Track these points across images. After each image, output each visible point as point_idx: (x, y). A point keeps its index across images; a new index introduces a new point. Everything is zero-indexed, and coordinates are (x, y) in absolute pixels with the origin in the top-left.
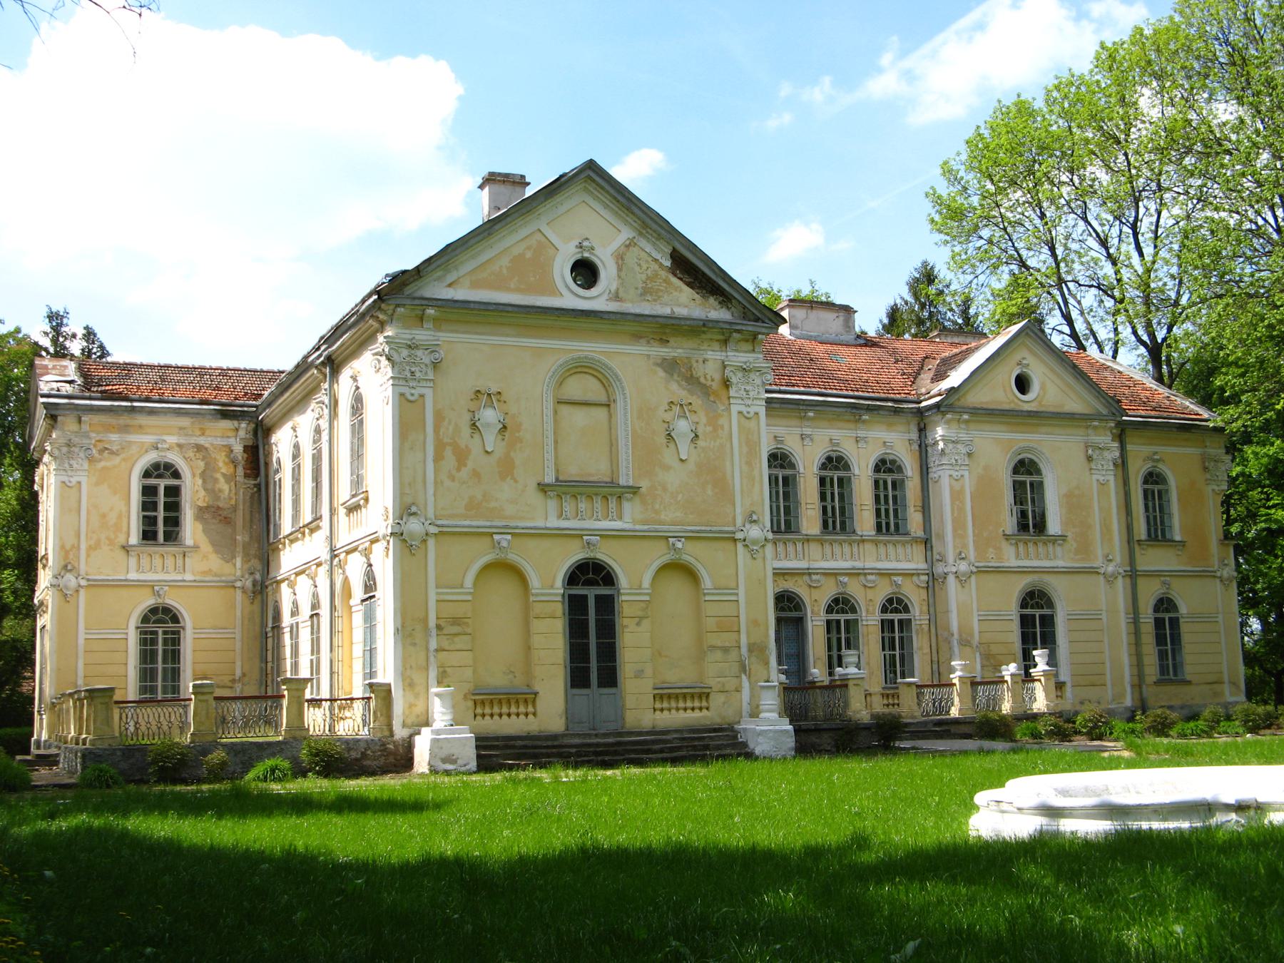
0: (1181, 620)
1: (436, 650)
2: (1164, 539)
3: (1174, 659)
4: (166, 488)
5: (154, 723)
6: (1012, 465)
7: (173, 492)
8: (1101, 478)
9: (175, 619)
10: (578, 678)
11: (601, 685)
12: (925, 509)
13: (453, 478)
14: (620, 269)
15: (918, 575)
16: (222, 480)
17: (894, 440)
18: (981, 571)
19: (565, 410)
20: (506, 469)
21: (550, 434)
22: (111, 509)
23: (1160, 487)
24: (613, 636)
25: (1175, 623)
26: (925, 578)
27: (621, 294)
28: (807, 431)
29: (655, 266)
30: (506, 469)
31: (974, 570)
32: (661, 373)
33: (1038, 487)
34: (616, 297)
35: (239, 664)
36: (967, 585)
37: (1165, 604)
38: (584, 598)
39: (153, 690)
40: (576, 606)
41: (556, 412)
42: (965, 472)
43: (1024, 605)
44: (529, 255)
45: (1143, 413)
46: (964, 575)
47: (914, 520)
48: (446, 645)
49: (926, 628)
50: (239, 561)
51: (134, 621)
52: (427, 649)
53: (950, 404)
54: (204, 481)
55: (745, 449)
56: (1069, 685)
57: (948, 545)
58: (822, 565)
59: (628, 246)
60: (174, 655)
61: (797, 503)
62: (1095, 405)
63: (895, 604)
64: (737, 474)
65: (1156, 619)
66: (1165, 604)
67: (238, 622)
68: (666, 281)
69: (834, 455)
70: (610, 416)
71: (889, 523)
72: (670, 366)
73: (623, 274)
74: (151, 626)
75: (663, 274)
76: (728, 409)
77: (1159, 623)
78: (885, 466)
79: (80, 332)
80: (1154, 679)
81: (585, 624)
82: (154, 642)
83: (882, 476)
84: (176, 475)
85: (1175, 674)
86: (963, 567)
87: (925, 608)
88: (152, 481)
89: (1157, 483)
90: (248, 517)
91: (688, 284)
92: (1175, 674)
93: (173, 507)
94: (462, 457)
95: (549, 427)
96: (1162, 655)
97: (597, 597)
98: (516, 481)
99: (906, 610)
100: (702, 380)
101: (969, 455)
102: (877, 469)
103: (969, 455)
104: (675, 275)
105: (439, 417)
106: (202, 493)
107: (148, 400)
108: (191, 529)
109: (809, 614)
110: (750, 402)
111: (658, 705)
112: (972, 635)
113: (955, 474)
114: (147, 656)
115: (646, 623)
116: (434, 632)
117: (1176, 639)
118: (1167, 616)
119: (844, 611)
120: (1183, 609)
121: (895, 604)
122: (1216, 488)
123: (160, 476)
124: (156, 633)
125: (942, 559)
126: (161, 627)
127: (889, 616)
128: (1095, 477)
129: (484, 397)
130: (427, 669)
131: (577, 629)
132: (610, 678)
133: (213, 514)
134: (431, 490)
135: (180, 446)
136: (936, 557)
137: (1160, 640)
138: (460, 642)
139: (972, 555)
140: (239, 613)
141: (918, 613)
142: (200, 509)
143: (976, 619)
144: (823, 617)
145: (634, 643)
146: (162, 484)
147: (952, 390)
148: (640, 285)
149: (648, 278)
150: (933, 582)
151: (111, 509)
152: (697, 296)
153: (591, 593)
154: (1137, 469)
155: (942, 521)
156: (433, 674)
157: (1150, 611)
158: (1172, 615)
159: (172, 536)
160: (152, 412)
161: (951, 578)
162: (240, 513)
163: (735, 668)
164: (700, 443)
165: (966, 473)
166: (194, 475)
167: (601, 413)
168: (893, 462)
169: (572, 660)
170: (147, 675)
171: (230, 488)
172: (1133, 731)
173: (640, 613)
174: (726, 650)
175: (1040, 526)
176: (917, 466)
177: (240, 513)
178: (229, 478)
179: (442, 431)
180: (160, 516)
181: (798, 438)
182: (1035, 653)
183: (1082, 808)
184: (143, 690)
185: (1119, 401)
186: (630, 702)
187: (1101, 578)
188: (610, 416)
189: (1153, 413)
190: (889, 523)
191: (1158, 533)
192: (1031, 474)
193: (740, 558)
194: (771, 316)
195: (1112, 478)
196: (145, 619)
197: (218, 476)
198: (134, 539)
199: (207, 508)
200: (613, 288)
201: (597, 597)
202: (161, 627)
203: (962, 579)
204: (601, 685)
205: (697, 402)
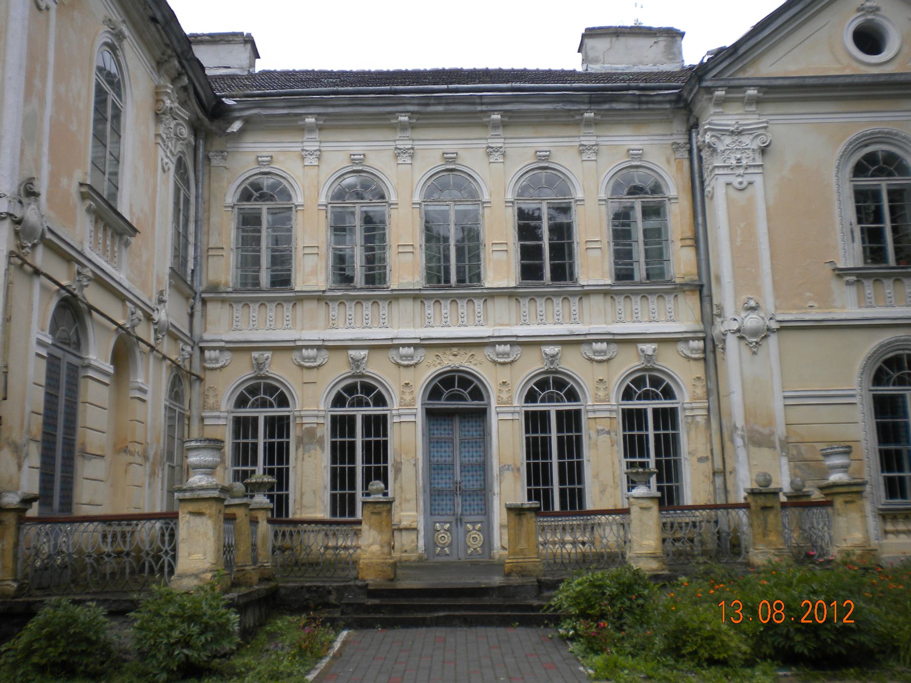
15: (686, 340)
17: (649, 147)
18: (785, 328)
26: (701, 344)
28: (497, 143)
31: (774, 325)
36: (762, 351)
38: (545, 415)
43: (879, 378)
46: (755, 333)
47: (681, 262)
49: (701, 420)
55: (563, 205)
57: (726, 295)
63: (649, 383)
86: (752, 321)
87: (700, 391)
97: (559, 413)
99: (668, 393)
101: (763, 151)
109: (494, 403)
110: (741, 171)
111: (889, 527)
112: (771, 421)
113: (736, 181)
121: (649, 383)
139: (769, 303)
141: (688, 396)
144: (518, 404)
150: (710, 351)
161: (732, 342)
172: (569, 583)
181: (482, 152)
192: (890, 174)
203: (754, 339)
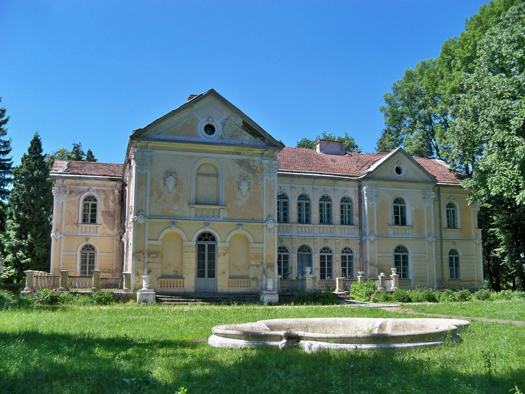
0: (460, 258)
1: (147, 263)
2: (454, 227)
3: (456, 271)
4: (92, 204)
5: (84, 283)
6: (393, 200)
7: (94, 206)
8: (428, 206)
9: (93, 249)
10: (200, 274)
11: (209, 277)
12: (360, 215)
13: (156, 202)
14: (223, 128)
16: (111, 202)
19: (200, 178)
20: (176, 199)
21: (194, 188)
22: (73, 211)
23: (453, 209)
24: (214, 260)
25: (457, 259)
27: (223, 136)
29: (236, 127)
30: (176, 199)
32: (237, 165)
33: (403, 209)
34: (221, 138)
35: (114, 264)
37: (453, 252)
39: (85, 273)
40: (200, 249)
41: (196, 179)
42: (372, 204)
44: (189, 123)
45: (448, 182)
47: (356, 219)
48: (151, 260)
49: (358, 259)
50: (115, 230)
51: (79, 249)
52: (144, 262)
53: (369, 176)
54: (104, 202)
56: (412, 280)
58: (299, 234)
59: (227, 120)
60: (92, 261)
61: (311, 213)
62: (428, 178)
64: (265, 202)
65: (450, 257)
66: (453, 252)
67: (115, 251)
68: (241, 132)
69: (325, 196)
70: (217, 180)
71: (346, 220)
72: (241, 163)
73: (224, 130)
74: (85, 251)
75: (240, 129)
76: (262, 178)
77: (451, 259)
78: (345, 200)
79: (86, 153)
80: (448, 279)
81: (204, 255)
82: (86, 256)
83: (344, 203)
84: (95, 200)
85: (457, 277)
88: (87, 202)
89: (452, 207)
90: (120, 215)
91: (249, 133)
92: (457, 277)
93: (94, 211)
94: (160, 194)
95: (194, 184)
96: (451, 271)
97: (209, 245)
98: (180, 203)
100: (253, 167)
102: (342, 201)
103: (376, 196)
104: (244, 130)
105: (152, 180)
106: (103, 207)
107: (86, 174)
108: (99, 218)
114: (84, 261)
115: (227, 255)
116: (147, 256)
117: (457, 265)
118: (454, 256)
119: (348, 252)
120: (460, 253)
122: (475, 209)
123: (90, 200)
124: (86, 254)
125: (365, 235)
126: (89, 252)
127: (344, 254)
128: (426, 205)
129: (169, 173)
130: (144, 269)
131: (200, 257)
132: (212, 274)
133: (106, 213)
134: (148, 206)
135: (96, 190)
136: (363, 233)
137: (451, 265)
138: (157, 260)
140: (115, 248)
142: (103, 212)
143: (376, 257)
145: (222, 263)
146: (91, 203)
147: (370, 172)
148: (231, 133)
149: (234, 131)
151: (73, 211)
152: (252, 138)
153: (207, 244)
154: (444, 203)
155: (365, 220)
156: (146, 271)
157: (448, 253)
158: (456, 256)
159: (93, 221)
160: (87, 179)
162: (117, 214)
163: (261, 272)
164: (251, 190)
165: (375, 203)
166: (101, 200)
167: (214, 179)
168: (348, 198)
169: (198, 268)
170: (83, 268)
171: (113, 205)
173: (225, 252)
174: (257, 266)
175: (404, 223)
176: (357, 200)
177: (117, 214)
178: (113, 201)
179: (153, 185)
180: (90, 216)
182: (392, 269)
183: (232, 335)
184: (82, 273)
185: (435, 177)
186: (220, 283)
187: (427, 242)
188: (217, 180)
189: (451, 182)
190: (346, 220)
191: (452, 225)
193: (265, 233)
194: (280, 145)
195: (432, 205)
196: (83, 249)
197: (110, 200)
198: (80, 221)
199: (105, 211)
200: (220, 134)
201: (209, 245)
202: (89, 252)
204: (209, 277)
205: (250, 175)
